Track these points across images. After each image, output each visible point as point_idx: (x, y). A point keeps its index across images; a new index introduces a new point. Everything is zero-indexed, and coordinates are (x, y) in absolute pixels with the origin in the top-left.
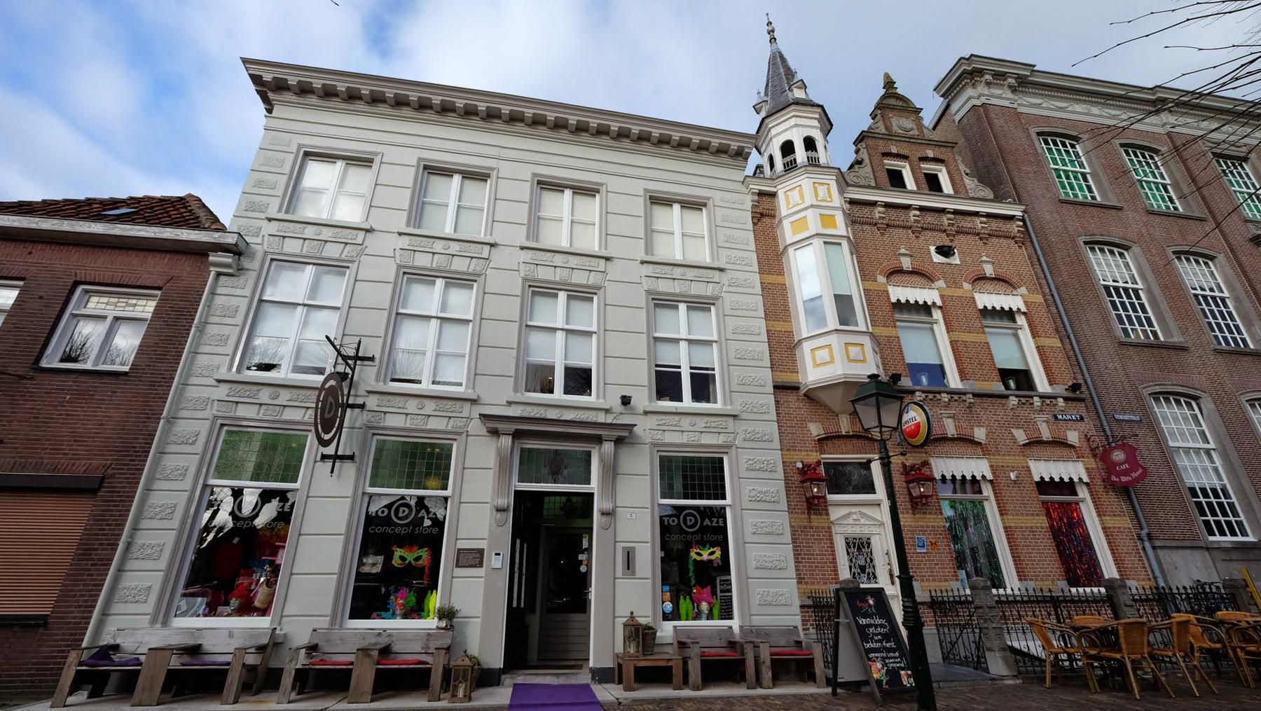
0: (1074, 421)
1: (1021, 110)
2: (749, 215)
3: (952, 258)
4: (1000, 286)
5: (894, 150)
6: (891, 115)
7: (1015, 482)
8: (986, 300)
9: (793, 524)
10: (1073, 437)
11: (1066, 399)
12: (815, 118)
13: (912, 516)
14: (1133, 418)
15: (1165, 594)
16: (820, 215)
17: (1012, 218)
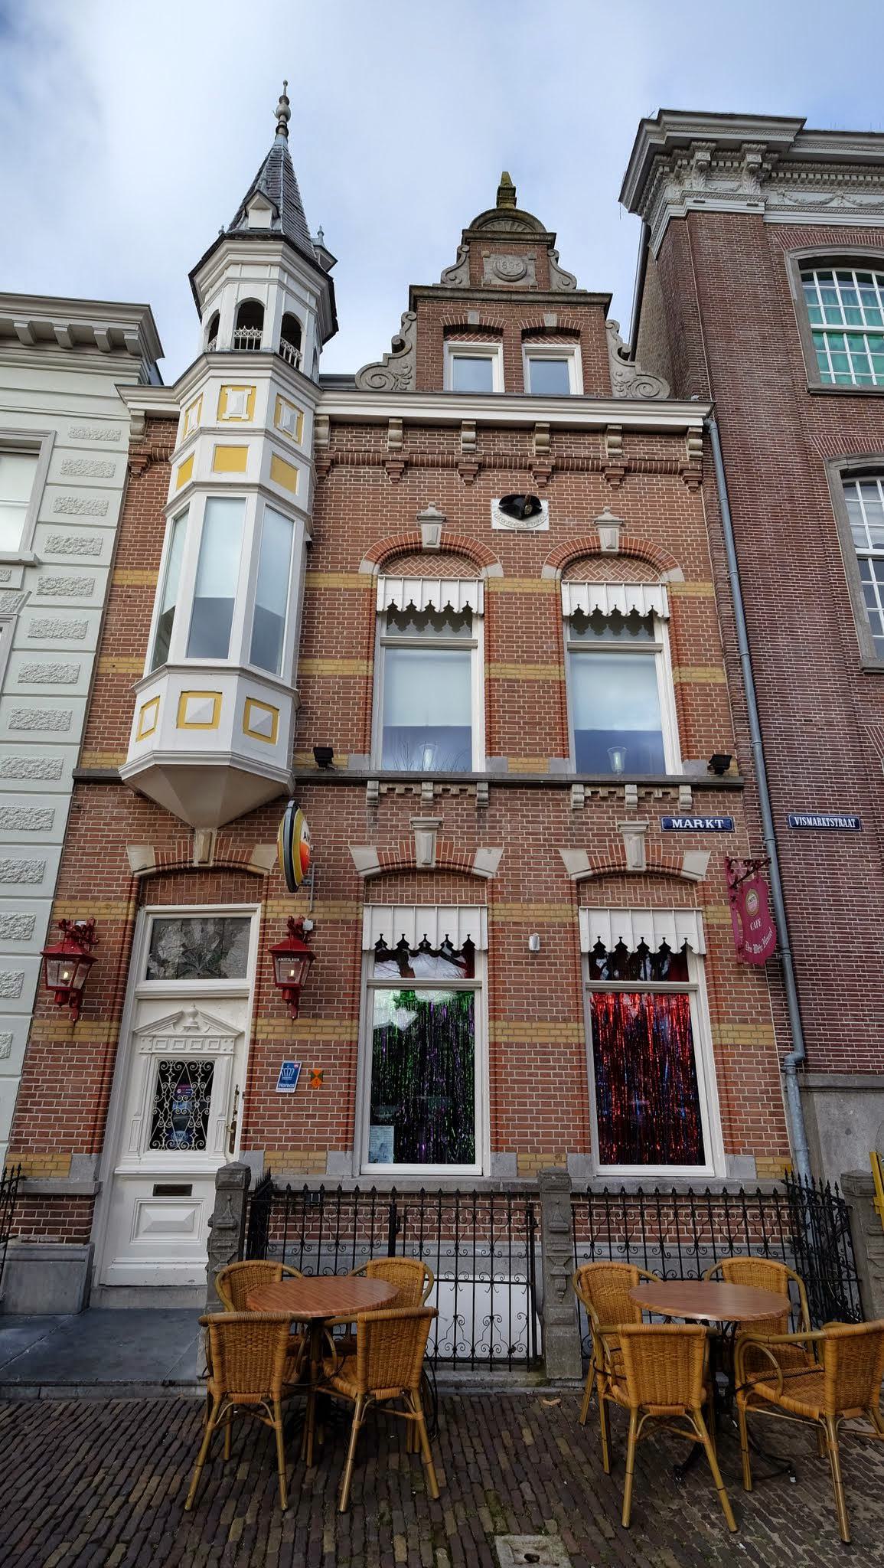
0: (710, 830)
1: (773, 217)
2: (124, 460)
3: (534, 519)
4: (630, 569)
5: (473, 318)
6: (484, 253)
7: (535, 955)
8: (579, 597)
9: (35, 1038)
10: (696, 863)
11: (696, 787)
12: (272, 264)
13: (289, 1022)
14: (842, 823)
15: (801, 1189)
16: (274, 454)
17: (681, 433)
